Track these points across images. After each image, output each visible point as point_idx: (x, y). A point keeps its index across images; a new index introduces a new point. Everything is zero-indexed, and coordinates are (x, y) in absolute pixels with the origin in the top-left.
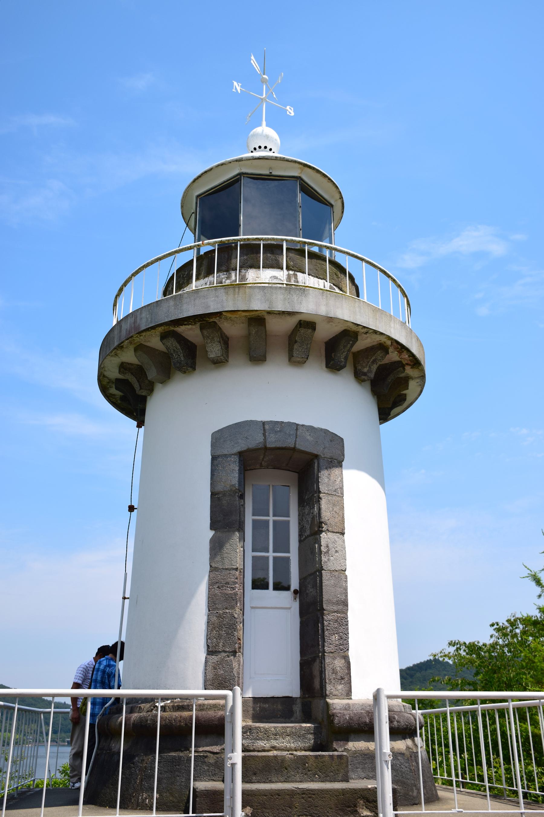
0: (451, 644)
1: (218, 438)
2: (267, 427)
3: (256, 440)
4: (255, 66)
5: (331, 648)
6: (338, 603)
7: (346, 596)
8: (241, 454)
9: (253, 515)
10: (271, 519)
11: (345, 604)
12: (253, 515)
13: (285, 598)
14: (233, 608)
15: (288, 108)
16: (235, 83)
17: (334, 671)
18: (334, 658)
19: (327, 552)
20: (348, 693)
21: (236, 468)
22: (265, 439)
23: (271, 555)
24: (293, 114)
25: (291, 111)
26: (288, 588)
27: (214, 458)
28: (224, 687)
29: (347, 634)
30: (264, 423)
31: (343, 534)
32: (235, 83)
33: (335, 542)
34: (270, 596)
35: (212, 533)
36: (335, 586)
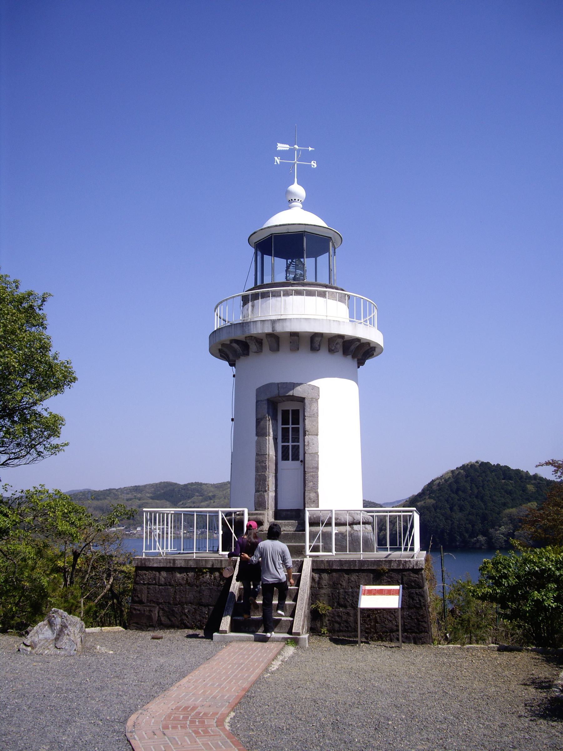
0: (553, 460)
1: (259, 391)
2: (280, 386)
3: (275, 392)
4: (284, 149)
5: (309, 488)
6: (313, 468)
7: (318, 465)
8: (268, 400)
9: (282, 425)
10: (290, 426)
11: (317, 468)
12: (282, 425)
13: (298, 463)
14: (265, 472)
15: (312, 162)
16: (276, 158)
17: (310, 499)
18: (310, 493)
19: (308, 445)
20: (316, 502)
21: (266, 406)
22: (279, 393)
23: (290, 444)
24: (316, 166)
25: (314, 164)
26: (298, 460)
27: (257, 402)
28: (521, 477)
29: (317, 482)
30: (278, 384)
31: (317, 435)
32: (276, 158)
33: (313, 440)
34: (290, 464)
35: (257, 438)
36: (312, 460)
